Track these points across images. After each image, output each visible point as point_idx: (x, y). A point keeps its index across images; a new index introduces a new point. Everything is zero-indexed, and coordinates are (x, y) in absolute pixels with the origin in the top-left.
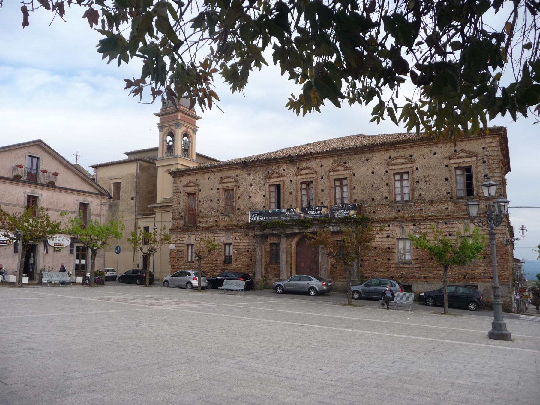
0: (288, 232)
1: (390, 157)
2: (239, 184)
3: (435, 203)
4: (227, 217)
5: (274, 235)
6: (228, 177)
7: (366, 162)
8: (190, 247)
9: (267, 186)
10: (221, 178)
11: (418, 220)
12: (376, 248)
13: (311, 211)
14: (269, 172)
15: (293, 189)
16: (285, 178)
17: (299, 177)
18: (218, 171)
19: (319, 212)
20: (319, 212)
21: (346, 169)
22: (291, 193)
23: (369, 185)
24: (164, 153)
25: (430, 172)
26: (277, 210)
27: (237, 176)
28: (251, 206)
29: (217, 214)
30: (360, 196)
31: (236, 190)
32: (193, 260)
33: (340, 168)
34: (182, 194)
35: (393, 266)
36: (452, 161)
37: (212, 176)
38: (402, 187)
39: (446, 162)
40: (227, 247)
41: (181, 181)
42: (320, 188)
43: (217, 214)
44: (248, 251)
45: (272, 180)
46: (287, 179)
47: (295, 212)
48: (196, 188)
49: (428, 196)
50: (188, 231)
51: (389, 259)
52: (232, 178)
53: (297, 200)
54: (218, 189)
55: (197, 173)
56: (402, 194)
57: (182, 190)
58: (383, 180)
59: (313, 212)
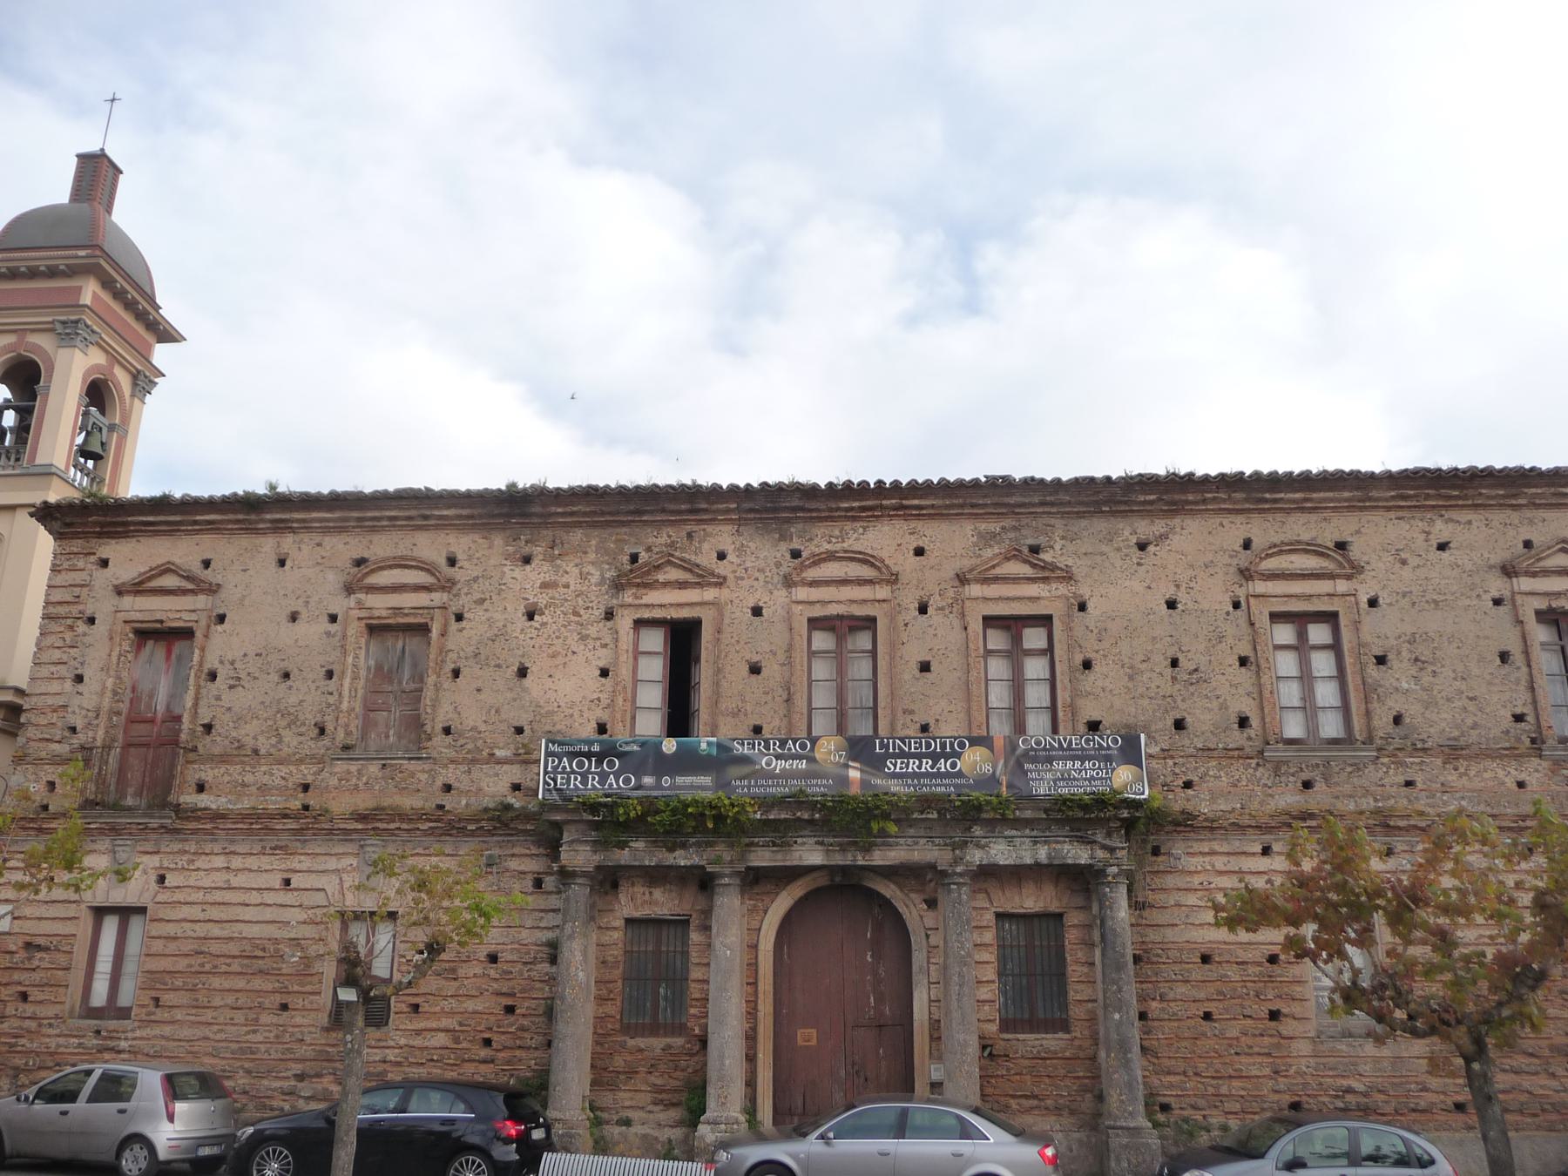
0: (762, 858)
2: (464, 602)
3: (1468, 758)
4: (374, 768)
5: (656, 876)
6: (401, 563)
8: (110, 926)
9: (625, 622)
11: (1407, 829)
12: (1206, 959)
13: (902, 755)
14: (634, 558)
15: (767, 648)
16: (723, 594)
17: (802, 593)
18: (341, 530)
19: (943, 765)
20: (943, 765)
21: (1049, 573)
22: (755, 670)
25: (1432, 622)
26: (670, 746)
27: (452, 562)
30: (1118, 703)
32: (124, 1000)
34: (101, 627)
35: (1303, 1047)
36: (1525, 584)
38: (1306, 678)
39: (1498, 586)
41: (104, 563)
42: (914, 653)
45: (653, 597)
46: (738, 598)
48: (201, 601)
49: (1437, 724)
50: (114, 831)
51: (1274, 1015)
54: (333, 618)
55: (213, 528)
56: (1309, 707)
57: (103, 605)
58: (1221, 638)
59: (913, 765)
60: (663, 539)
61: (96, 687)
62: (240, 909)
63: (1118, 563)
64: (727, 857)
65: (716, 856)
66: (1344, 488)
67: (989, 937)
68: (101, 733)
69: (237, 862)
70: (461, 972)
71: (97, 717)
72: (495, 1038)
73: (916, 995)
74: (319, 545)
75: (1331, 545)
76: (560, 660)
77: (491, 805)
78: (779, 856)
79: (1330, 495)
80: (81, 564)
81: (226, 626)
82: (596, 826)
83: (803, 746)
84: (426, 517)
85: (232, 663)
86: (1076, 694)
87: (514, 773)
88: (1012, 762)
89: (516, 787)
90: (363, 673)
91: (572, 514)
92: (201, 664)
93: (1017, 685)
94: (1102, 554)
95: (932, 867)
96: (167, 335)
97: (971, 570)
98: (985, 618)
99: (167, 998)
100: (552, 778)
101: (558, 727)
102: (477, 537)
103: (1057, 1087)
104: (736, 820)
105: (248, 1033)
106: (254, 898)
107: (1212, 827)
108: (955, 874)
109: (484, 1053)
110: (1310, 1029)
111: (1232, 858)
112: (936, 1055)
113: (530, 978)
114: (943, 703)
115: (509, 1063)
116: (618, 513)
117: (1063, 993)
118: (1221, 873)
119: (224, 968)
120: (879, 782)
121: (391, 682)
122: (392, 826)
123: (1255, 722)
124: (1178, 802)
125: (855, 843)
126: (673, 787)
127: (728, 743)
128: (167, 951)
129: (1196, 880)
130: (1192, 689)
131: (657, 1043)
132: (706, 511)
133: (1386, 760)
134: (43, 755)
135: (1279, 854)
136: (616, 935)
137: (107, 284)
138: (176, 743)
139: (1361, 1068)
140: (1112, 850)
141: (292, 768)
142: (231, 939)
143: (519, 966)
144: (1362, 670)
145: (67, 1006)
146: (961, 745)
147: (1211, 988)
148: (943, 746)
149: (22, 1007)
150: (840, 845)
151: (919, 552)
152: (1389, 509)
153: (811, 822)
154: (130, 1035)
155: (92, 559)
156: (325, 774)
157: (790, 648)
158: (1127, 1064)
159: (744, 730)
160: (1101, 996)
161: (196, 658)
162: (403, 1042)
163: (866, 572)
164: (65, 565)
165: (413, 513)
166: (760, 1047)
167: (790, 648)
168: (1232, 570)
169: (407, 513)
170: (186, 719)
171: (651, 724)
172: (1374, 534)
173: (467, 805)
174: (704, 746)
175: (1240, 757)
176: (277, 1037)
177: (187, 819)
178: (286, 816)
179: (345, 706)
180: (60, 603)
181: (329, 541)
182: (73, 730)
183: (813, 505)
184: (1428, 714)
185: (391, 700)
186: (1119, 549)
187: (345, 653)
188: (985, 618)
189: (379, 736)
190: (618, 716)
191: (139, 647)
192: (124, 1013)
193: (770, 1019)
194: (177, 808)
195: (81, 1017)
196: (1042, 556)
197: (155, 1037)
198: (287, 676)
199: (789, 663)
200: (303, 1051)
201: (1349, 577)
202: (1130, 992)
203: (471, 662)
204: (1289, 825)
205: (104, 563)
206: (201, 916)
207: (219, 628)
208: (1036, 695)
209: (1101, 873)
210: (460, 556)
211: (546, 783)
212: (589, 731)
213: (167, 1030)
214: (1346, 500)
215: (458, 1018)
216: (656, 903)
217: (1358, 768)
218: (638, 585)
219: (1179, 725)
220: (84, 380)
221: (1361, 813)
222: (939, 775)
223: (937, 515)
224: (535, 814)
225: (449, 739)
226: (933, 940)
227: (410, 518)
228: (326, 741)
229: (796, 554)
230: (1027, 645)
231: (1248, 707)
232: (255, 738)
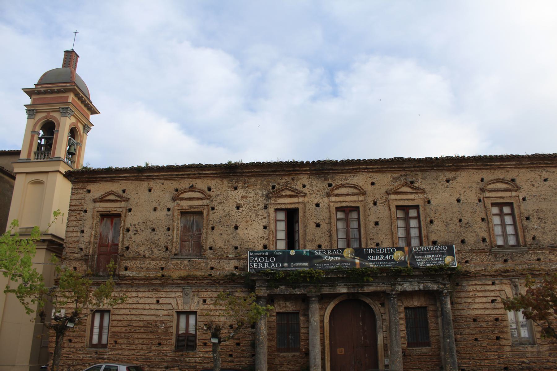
0: (326, 291)
1: (482, 180)
4: (186, 262)
5: (286, 298)
7: (446, 184)
9: (272, 210)
10: (177, 190)
12: (475, 320)
14: (273, 187)
16: (306, 199)
17: (333, 199)
18: (170, 179)
19: (387, 257)
20: (387, 257)
21: (418, 191)
22: (318, 225)
23: (454, 219)
24: (32, 155)
25: (544, 205)
27: (209, 189)
28: (237, 244)
29: (163, 254)
30: (442, 234)
31: (208, 215)
32: (104, 341)
33: (405, 189)
34: (89, 214)
35: (508, 349)
37: (156, 185)
38: (503, 225)
40: (183, 319)
42: (373, 219)
43: (163, 254)
47: (342, 256)
48: (123, 204)
51: (498, 338)
52: (202, 192)
53: (330, 236)
54: (169, 210)
55: (126, 179)
56: (505, 235)
57: (89, 206)
58: (475, 212)
59: (377, 258)
60: (283, 181)
61: (88, 234)
62: (142, 311)
63: (440, 187)
64: (314, 290)
65: (310, 291)
66: (514, 161)
67: (402, 315)
68: (91, 250)
69: (140, 295)
71: (89, 245)
72: (234, 354)
73: (379, 336)
74: (163, 184)
75: (509, 180)
76: (249, 223)
77: (228, 274)
78: (332, 290)
79: (509, 163)
80: (81, 192)
81: (132, 213)
82: (268, 281)
83: (339, 252)
84: (200, 174)
85: (135, 225)
86: (428, 232)
87: (235, 263)
88: (411, 256)
89: (236, 268)
90: (180, 228)
91: (252, 172)
92: (124, 226)
93: (408, 229)
94: (435, 184)
95: (384, 292)
96: (94, 111)
97: (391, 190)
98: (397, 206)
99: (120, 341)
100: (251, 265)
101: (250, 247)
102: (218, 181)
103: (428, 365)
104: (317, 278)
105: (148, 353)
106: (147, 307)
107: (476, 276)
108: (392, 294)
109: (230, 359)
110: (510, 342)
111: (482, 286)
112: (386, 356)
113: (245, 333)
114: (384, 236)
115: (239, 362)
116: (267, 172)
117: (427, 333)
118: (479, 291)
119: (138, 331)
120: (366, 263)
121: (189, 232)
122: (194, 282)
123: (488, 240)
124: (464, 268)
125: (358, 285)
126: (295, 267)
127: (313, 251)
128: (118, 325)
129: (471, 294)
130: (467, 229)
131: (290, 354)
132: (298, 170)
133: (531, 252)
134: (72, 257)
135: (498, 284)
136: (274, 318)
137: (77, 95)
138: (117, 253)
139: (527, 355)
140: (445, 285)
141: (157, 262)
142: (140, 321)
144: (520, 222)
145: (85, 344)
146: (394, 250)
147: (477, 330)
148: (387, 251)
149: (70, 344)
150: (352, 285)
151: (373, 184)
152: (528, 168)
153: (343, 278)
154: (108, 353)
155: (85, 190)
156: (169, 264)
157: (330, 218)
158: (452, 356)
159: (315, 247)
160: (441, 334)
161: (122, 224)
162: (202, 355)
163: (355, 191)
164: (76, 192)
165: (196, 172)
166: (326, 355)
167: (330, 218)
168: (478, 189)
169: (194, 173)
170: (120, 245)
171: (282, 245)
172: (524, 176)
173: (219, 274)
174: (305, 252)
175: (483, 252)
176: (158, 354)
177: (123, 280)
178: (157, 279)
179: (175, 240)
180: (75, 205)
181: (166, 183)
182: (81, 249)
183: (336, 168)
184: (544, 236)
185: (190, 238)
186: (440, 182)
187: (174, 222)
188: (397, 206)
189: (186, 250)
190: (271, 242)
191: (101, 220)
192: (105, 346)
193: (329, 345)
194: (119, 275)
195: (89, 347)
196: (415, 185)
197: (116, 354)
198: (153, 230)
199: (330, 223)
200: (167, 359)
201: (516, 191)
202: (452, 332)
203: (218, 224)
204: (501, 275)
205: (89, 191)
206: (129, 313)
207: (129, 213)
208: (414, 233)
209: (442, 292)
210: (212, 187)
211: (250, 266)
212: (260, 248)
213: (120, 352)
214: (514, 165)
216: (287, 307)
217: (522, 255)
218: (276, 197)
219: (463, 242)
220: (70, 125)
221: (524, 270)
222: (386, 261)
223: (379, 171)
224: (244, 277)
225: (212, 251)
226: (384, 317)
227: (194, 174)
228: (169, 253)
229: (330, 185)
230: (411, 215)
231: (485, 235)
232: (144, 252)
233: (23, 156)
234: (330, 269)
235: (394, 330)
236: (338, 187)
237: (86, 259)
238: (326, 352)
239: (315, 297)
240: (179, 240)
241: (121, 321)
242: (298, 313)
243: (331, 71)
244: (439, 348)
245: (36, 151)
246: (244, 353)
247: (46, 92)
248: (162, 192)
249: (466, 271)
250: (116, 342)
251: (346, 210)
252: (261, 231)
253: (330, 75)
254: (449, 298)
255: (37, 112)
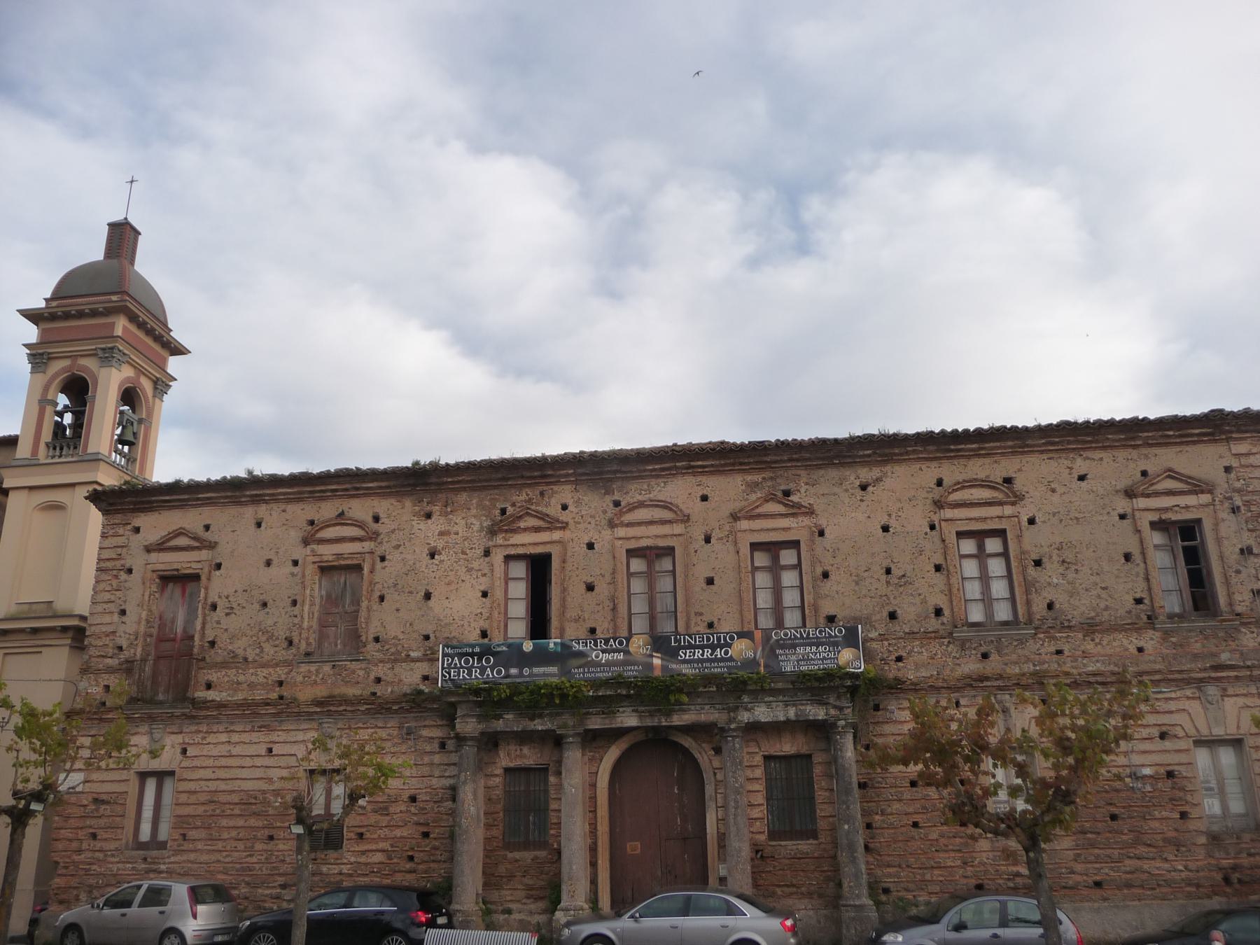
0: (595, 723)
1: (939, 483)
4: (327, 668)
5: (524, 738)
7: (859, 493)
9: (498, 557)
10: (312, 523)
14: (503, 511)
16: (567, 535)
17: (621, 532)
18: (299, 500)
21: (797, 510)
22: (590, 588)
27: (376, 519)
28: (429, 630)
29: (283, 654)
32: (163, 835)
37: (271, 514)
38: (985, 578)
42: (702, 572)
43: (283, 654)
44: (413, 799)
47: (627, 652)
48: (204, 554)
53: (614, 609)
54: (295, 563)
55: (209, 502)
56: (987, 600)
57: (137, 560)
59: (698, 653)
60: (523, 497)
65: (564, 723)
66: (1007, 439)
67: (759, 773)
68: (139, 650)
69: (235, 738)
70: (392, 810)
72: (416, 855)
74: (284, 511)
75: (1000, 480)
76: (453, 587)
78: (607, 721)
80: (121, 531)
81: (222, 571)
82: (480, 704)
83: (621, 643)
84: (357, 489)
86: (817, 596)
87: (424, 668)
88: (767, 649)
91: (459, 482)
92: (206, 599)
96: (178, 350)
97: (740, 511)
99: (192, 834)
102: (393, 501)
106: (248, 762)
109: (409, 866)
113: (439, 812)
115: (426, 872)
119: (229, 812)
122: (341, 708)
123: (946, 612)
127: (569, 643)
128: (190, 801)
130: (901, 589)
131: (527, 856)
136: (498, 780)
137: (133, 318)
140: (841, 709)
142: (233, 791)
143: (431, 804)
146: (732, 638)
148: (719, 639)
149: (92, 843)
152: (1042, 452)
153: (628, 696)
155: (129, 527)
156: (293, 674)
162: (353, 859)
163: (667, 515)
164: (111, 532)
168: (929, 502)
170: (197, 638)
171: (518, 629)
172: (1032, 472)
175: (936, 638)
177: (200, 708)
178: (268, 704)
179: (306, 624)
182: (120, 648)
186: (847, 490)
191: (163, 588)
192: (162, 846)
194: (194, 702)
198: (265, 605)
199: (613, 582)
200: (284, 868)
201: (1013, 504)
204: (971, 685)
205: (137, 530)
206: (212, 776)
207: (217, 573)
208: (791, 598)
209: (834, 725)
212: (473, 636)
213: (192, 856)
215: (390, 842)
217: (1022, 642)
218: (506, 531)
219: (893, 616)
221: (1024, 675)
222: (716, 660)
225: (378, 646)
227: (346, 490)
228: (294, 650)
230: (783, 562)
231: (942, 601)
233: (23, 451)
234: (600, 679)
235: (732, 804)
236: (633, 508)
237: (128, 668)
238: (600, 849)
239: (573, 736)
240: (315, 624)
241: (195, 792)
242: (547, 769)
243: (791, 195)
244: (835, 844)
245: (49, 440)
246: (438, 852)
247: (67, 316)
248: (284, 524)
249: (896, 679)
250: (184, 835)
251: (652, 554)
252: (477, 603)
253: (789, 204)
254: (850, 737)
255: (49, 359)
